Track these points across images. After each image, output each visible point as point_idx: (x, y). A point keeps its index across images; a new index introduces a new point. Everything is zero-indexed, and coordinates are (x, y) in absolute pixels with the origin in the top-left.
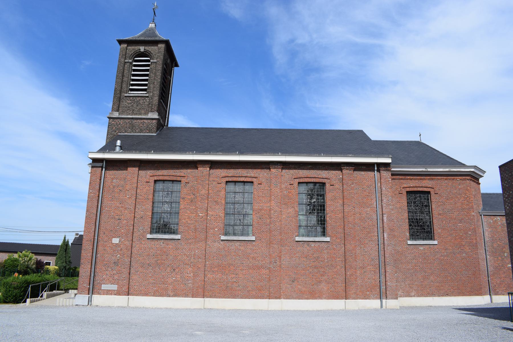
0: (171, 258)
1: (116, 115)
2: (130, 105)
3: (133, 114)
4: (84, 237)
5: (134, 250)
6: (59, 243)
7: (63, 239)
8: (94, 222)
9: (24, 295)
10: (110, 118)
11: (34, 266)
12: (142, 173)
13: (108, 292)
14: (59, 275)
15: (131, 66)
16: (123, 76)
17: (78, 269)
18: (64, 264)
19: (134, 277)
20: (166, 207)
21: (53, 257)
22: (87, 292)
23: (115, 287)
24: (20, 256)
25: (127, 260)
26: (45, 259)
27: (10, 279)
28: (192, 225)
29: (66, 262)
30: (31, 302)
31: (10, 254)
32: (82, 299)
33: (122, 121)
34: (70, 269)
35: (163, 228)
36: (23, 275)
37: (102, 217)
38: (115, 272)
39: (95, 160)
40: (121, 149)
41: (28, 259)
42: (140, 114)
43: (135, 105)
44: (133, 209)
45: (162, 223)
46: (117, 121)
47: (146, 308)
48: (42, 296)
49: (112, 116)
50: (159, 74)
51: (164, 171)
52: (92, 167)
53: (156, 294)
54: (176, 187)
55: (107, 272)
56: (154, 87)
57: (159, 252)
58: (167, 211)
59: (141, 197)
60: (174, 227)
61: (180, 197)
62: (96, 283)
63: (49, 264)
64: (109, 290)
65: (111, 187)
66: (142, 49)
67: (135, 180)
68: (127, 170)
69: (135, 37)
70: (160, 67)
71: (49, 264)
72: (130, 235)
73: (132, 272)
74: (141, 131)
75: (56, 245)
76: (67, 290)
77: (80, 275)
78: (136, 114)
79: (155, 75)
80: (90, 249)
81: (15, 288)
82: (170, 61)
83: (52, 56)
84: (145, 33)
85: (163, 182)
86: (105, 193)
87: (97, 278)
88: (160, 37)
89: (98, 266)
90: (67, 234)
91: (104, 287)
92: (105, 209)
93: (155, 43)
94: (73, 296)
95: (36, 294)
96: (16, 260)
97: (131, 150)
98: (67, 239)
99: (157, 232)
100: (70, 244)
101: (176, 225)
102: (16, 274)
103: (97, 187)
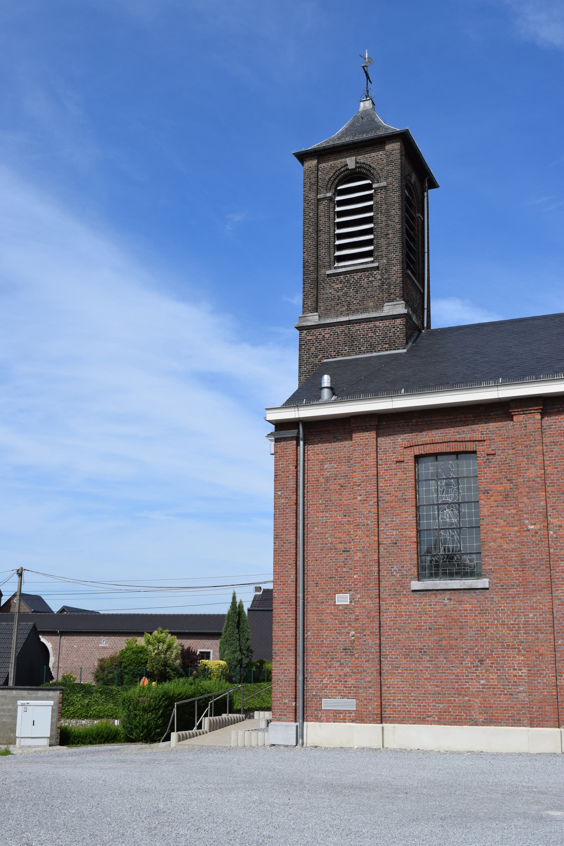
0: (471, 632)
1: (313, 319)
2: (340, 293)
3: (349, 311)
4: (275, 595)
5: (385, 617)
6: (224, 609)
7: (231, 600)
8: (292, 561)
9: (165, 723)
10: (300, 329)
11: (178, 661)
12: (386, 442)
13: (337, 716)
14: (230, 679)
15: (332, 205)
16: (318, 231)
17: (267, 666)
18: (238, 655)
19: (390, 680)
20: (448, 516)
21: (214, 641)
22: (292, 716)
23: (350, 704)
24: (148, 642)
25: (372, 642)
26: (199, 646)
27: (133, 692)
28: (514, 554)
29: (241, 650)
30: (180, 739)
31: (130, 638)
32: (283, 732)
33: (327, 330)
34: (250, 665)
35: (443, 562)
36: (159, 682)
37: (309, 547)
38: (348, 670)
39: (281, 426)
40: (334, 394)
41: (165, 646)
42: (366, 310)
43: (351, 293)
44: (372, 524)
45: (442, 552)
46: (316, 332)
47: (425, 752)
48: (200, 727)
49: (305, 324)
50: (396, 212)
51: (434, 432)
52: (277, 440)
53: (443, 719)
54: (466, 466)
55: (331, 671)
56: (388, 245)
57: (441, 621)
58: (452, 524)
59: (388, 498)
60: (471, 561)
61: (477, 489)
62: (308, 695)
63: (206, 655)
64: (339, 712)
65: (322, 480)
66: (351, 162)
67: (371, 460)
68: (351, 439)
69: (333, 140)
70: (395, 197)
71: (206, 655)
72: (373, 584)
73: (385, 668)
74: (372, 348)
75: (218, 615)
76: (248, 712)
77: (274, 678)
78: (357, 311)
79: (388, 216)
80: (290, 619)
81: (145, 710)
82: (417, 177)
83: (162, 215)
84: (352, 125)
85: (433, 458)
86: (309, 496)
87: (310, 684)
88: (387, 129)
89: (311, 658)
90: (238, 590)
91: (327, 704)
92: (314, 531)
93: (378, 143)
94: (263, 725)
95: (187, 722)
96: (142, 651)
97: (354, 393)
98: (238, 600)
99: (434, 575)
100: (246, 612)
101: (474, 556)
102: (145, 681)
103: (292, 483)
